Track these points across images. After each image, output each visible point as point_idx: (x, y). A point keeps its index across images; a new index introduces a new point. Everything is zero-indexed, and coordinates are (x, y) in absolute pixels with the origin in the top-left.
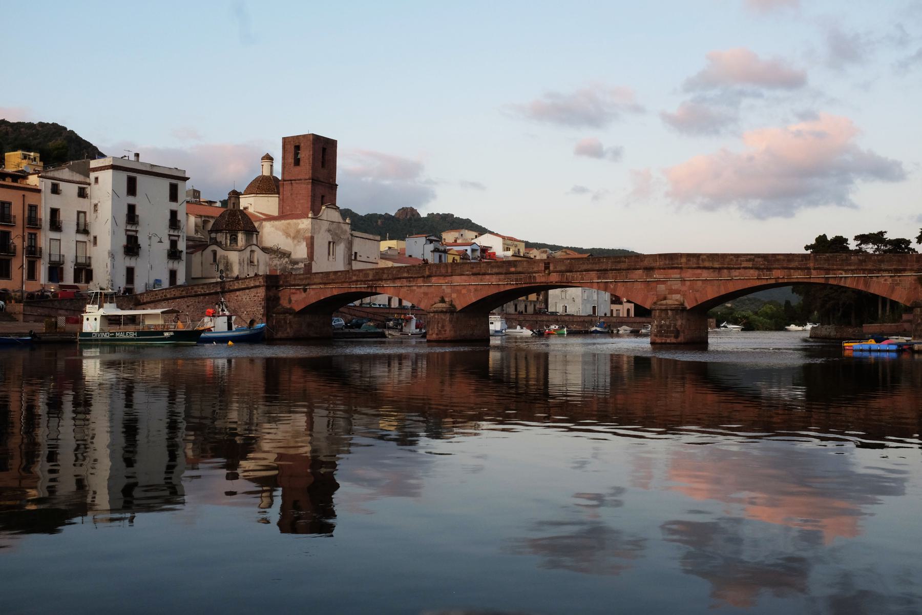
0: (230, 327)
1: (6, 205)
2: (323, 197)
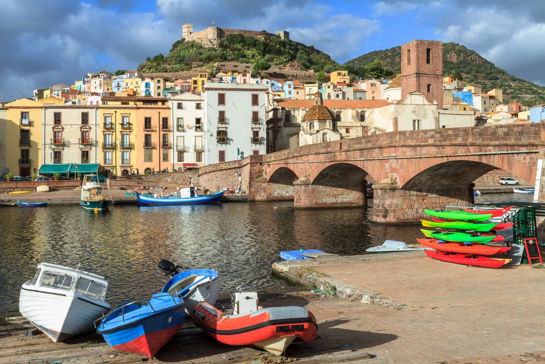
1: (148, 120)
2: (429, 86)
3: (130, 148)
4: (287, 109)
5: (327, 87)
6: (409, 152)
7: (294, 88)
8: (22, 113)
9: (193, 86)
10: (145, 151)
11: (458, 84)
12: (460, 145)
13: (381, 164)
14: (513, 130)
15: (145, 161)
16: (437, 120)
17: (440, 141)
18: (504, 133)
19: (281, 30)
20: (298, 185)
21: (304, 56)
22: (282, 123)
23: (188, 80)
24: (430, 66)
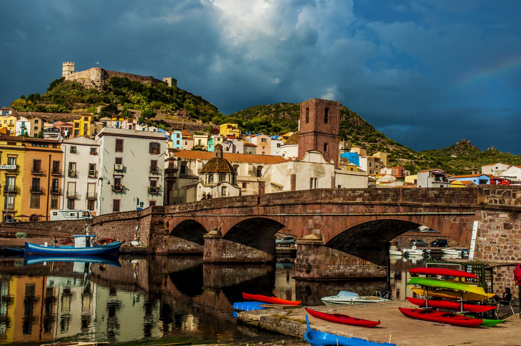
0: (88, 244)
2: (326, 145)
3: (15, 192)
4: (183, 160)
5: (216, 139)
6: (335, 210)
7: (183, 138)
8: (91, 149)
9: (74, 129)
10: (31, 197)
11: (345, 145)
12: (390, 205)
13: (304, 220)
14: (444, 193)
15: (31, 207)
16: (333, 180)
17: (369, 200)
18: (435, 195)
19: (168, 77)
20: (208, 238)
21: (192, 106)
22: (177, 174)
23: (69, 123)
24: (328, 126)
